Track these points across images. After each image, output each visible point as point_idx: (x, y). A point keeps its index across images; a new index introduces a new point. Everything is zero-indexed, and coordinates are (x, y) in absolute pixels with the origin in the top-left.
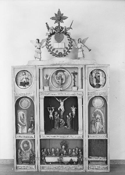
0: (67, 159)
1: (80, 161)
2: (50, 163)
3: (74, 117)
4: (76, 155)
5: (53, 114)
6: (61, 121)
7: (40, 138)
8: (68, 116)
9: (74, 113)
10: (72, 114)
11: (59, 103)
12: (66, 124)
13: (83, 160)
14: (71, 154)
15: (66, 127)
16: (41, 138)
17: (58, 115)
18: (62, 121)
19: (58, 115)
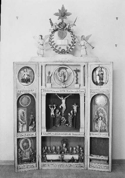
0: (68, 157)
1: (81, 159)
2: (51, 161)
3: (75, 115)
4: (76, 153)
5: (55, 111)
6: (62, 119)
7: (42, 136)
8: (69, 114)
9: (75, 110)
10: (73, 112)
11: (61, 100)
12: (67, 122)
13: (84, 158)
14: (72, 152)
15: (67, 125)
16: (43, 135)
17: (60, 113)
18: (63, 119)
19: (60, 113)
